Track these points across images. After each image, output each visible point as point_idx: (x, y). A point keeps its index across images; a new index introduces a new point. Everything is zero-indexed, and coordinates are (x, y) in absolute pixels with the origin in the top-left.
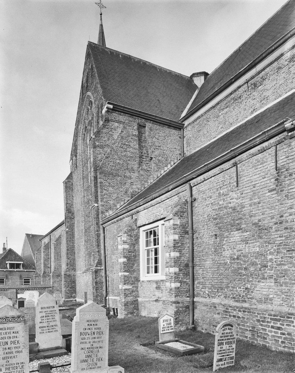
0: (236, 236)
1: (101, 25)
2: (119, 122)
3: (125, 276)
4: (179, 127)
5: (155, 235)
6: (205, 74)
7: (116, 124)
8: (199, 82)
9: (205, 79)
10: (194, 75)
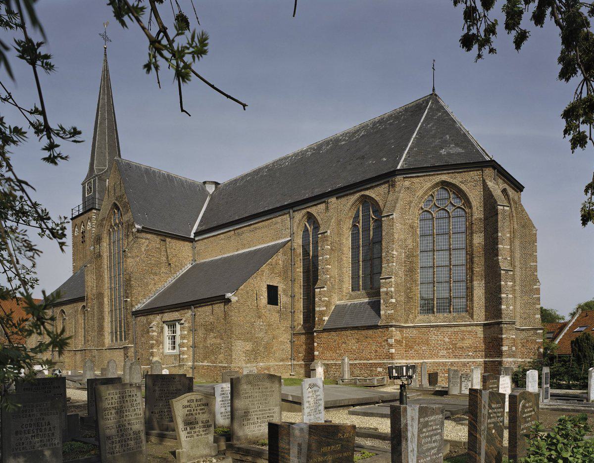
0: (212, 335)
1: (106, 71)
2: (147, 239)
3: (501, 318)
4: (191, 241)
5: (174, 328)
6: (216, 184)
7: (144, 240)
8: (211, 189)
9: (216, 187)
10: (205, 183)
